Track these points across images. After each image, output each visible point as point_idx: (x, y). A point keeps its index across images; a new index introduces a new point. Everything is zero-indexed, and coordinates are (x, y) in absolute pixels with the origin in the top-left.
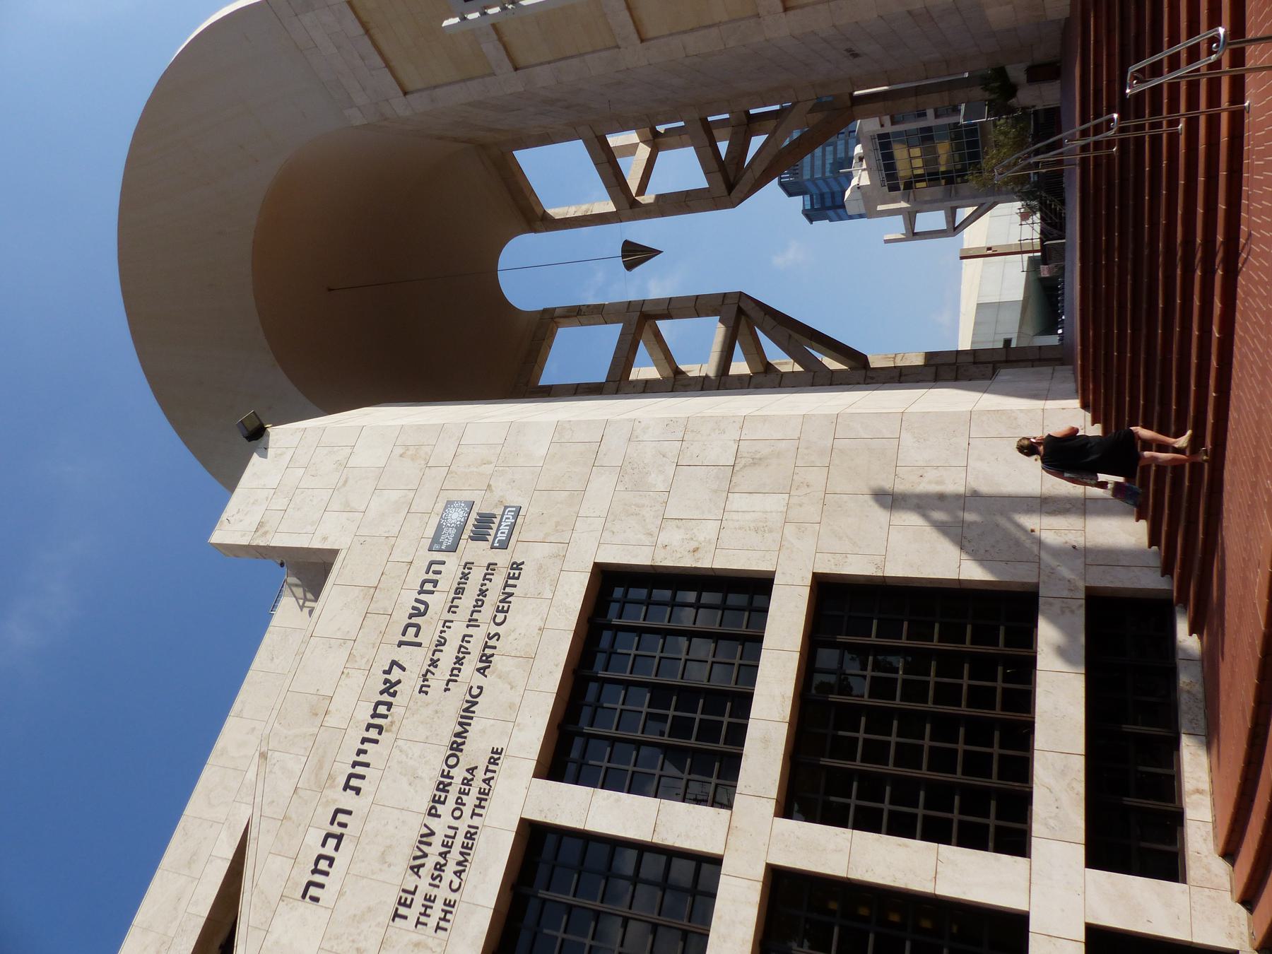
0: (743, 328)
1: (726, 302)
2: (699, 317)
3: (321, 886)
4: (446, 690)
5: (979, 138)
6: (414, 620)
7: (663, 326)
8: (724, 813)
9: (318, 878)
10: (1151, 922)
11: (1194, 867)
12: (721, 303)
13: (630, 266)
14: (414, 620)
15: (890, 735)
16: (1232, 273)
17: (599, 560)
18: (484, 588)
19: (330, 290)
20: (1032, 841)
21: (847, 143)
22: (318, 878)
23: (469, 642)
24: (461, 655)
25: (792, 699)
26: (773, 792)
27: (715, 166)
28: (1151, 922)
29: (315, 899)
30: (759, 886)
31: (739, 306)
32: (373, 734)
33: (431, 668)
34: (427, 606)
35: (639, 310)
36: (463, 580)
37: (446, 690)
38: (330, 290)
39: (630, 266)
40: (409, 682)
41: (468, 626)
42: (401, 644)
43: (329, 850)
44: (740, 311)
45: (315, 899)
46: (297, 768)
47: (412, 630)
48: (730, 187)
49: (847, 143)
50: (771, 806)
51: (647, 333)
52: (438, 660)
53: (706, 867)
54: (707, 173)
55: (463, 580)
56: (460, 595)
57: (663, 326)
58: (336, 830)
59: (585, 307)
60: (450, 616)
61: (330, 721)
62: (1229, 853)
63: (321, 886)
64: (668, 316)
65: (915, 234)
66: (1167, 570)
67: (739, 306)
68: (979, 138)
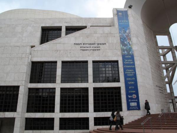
0: (171, 65)
7: (170, 52)
8: (92, 82)
10: (34, 46)
11: (95, 127)
15: (87, 111)
16: (157, 129)
20: (7, 117)
25: (78, 117)
26: (96, 87)
28: (34, 46)
30: (86, 87)
46: (88, 33)
50: (94, 87)
51: (169, 50)
53: (87, 81)
57: (170, 52)
61: (94, 34)
62: (97, 129)
64: (172, 53)
66: (126, 124)
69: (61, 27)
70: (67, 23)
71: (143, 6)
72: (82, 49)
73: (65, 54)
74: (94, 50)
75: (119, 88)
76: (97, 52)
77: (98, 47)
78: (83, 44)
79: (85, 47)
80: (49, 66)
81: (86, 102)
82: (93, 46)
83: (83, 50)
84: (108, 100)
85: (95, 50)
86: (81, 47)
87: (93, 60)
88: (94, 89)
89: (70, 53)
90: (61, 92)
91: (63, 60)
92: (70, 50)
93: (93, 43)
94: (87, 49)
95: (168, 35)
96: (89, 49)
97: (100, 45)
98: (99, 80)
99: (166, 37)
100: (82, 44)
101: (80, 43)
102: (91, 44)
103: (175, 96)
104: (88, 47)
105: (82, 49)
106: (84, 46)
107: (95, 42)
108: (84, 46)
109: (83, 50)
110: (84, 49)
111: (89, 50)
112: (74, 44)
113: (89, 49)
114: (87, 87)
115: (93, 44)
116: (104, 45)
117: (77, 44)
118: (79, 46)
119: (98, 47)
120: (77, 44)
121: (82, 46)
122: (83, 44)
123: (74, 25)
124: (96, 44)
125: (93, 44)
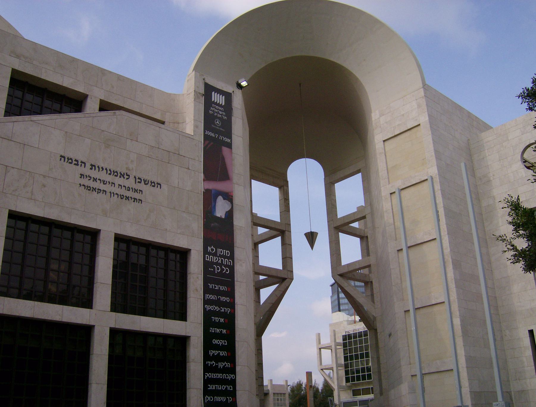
1: (289, 272)
2: (282, 259)
3: (64, 161)
4: (80, 184)
5: (367, 381)
6: (143, 181)
8: (109, 309)
9: (66, 160)
12: (288, 270)
13: (307, 235)
14: (143, 181)
17: (192, 252)
18: (130, 199)
19: (300, 84)
21: (347, 310)
22: (66, 160)
23: (103, 193)
24: (97, 190)
27: (351, 269)
29: (61, 159)
31: (287, 278)
32: (109, 172)
33: (92, 179)
34: (147, 184)
35: (286, 230)
36: (134, 190)
37: (80, 184)
38: (300, 84)
39: (307, 235)
40: (80, 169)
41: (110, 192)
42: (135, 177)
43: (74, 162)
44: (284, 279)
45: (61, 159)
47: (140, 181)
48: (341, 275)
49: (347, 310)
51: (274, 233)
52: (96, 181)
54: (348, 265)
55: (134, 190)
56: (127, 189)
58: (80, 163)
59: (288, 202)
60: (117, 186)
61: (129, 142)
63: (64, 161)
65: (320, 349)
67: (287, 278)
68: (367, 381)
69: (85, 97)
70: (18, 57)
71: (258, 73)
72: (86, 182)
73: (25, 186)
74: (122, 197)
75: (366, 380)
76: (131, 206)
77: (136, 191)
78: (92, 165)
79: (95, 180)
80: (69, 242)
81: (275, 402)
82: (119, 181)
83: (88, 188)
84: (283, 400)
85: (127, 198)
86: (82, 175)
87: (119, 232)
88: (114, 332)
89: (44, 186)
90: (112, 345)
91: (13, 208)
92: (44, 176)
93: (124, 171)
94: (102, 187)
95: (280, 188)
96: (107, 188)
97: (142, 186)
98: (351, 358)
99: (274, 192)
100: (88, 166)
101: (80, 158)
102: (115, 173)
103: (273, 384)
104: (104, 183)
105: (86, 182)
106: (94, 174)
107: (128, 169)
108: (94, 174)
109: (88, 188)
110: (92, 184)
111: (108, 194)
112: (61, 156)
113: (107, 188)
114: (92, 323)
115: (122, 175)
116: (156, 190)
117: (70, 160)
118: (74, 171)
119: (136, 191)
120: (70, 160)
121: (87, 171)
122: (92, 165)
123: (43, 77)
124: (132, 179)
125: (122, 175)
